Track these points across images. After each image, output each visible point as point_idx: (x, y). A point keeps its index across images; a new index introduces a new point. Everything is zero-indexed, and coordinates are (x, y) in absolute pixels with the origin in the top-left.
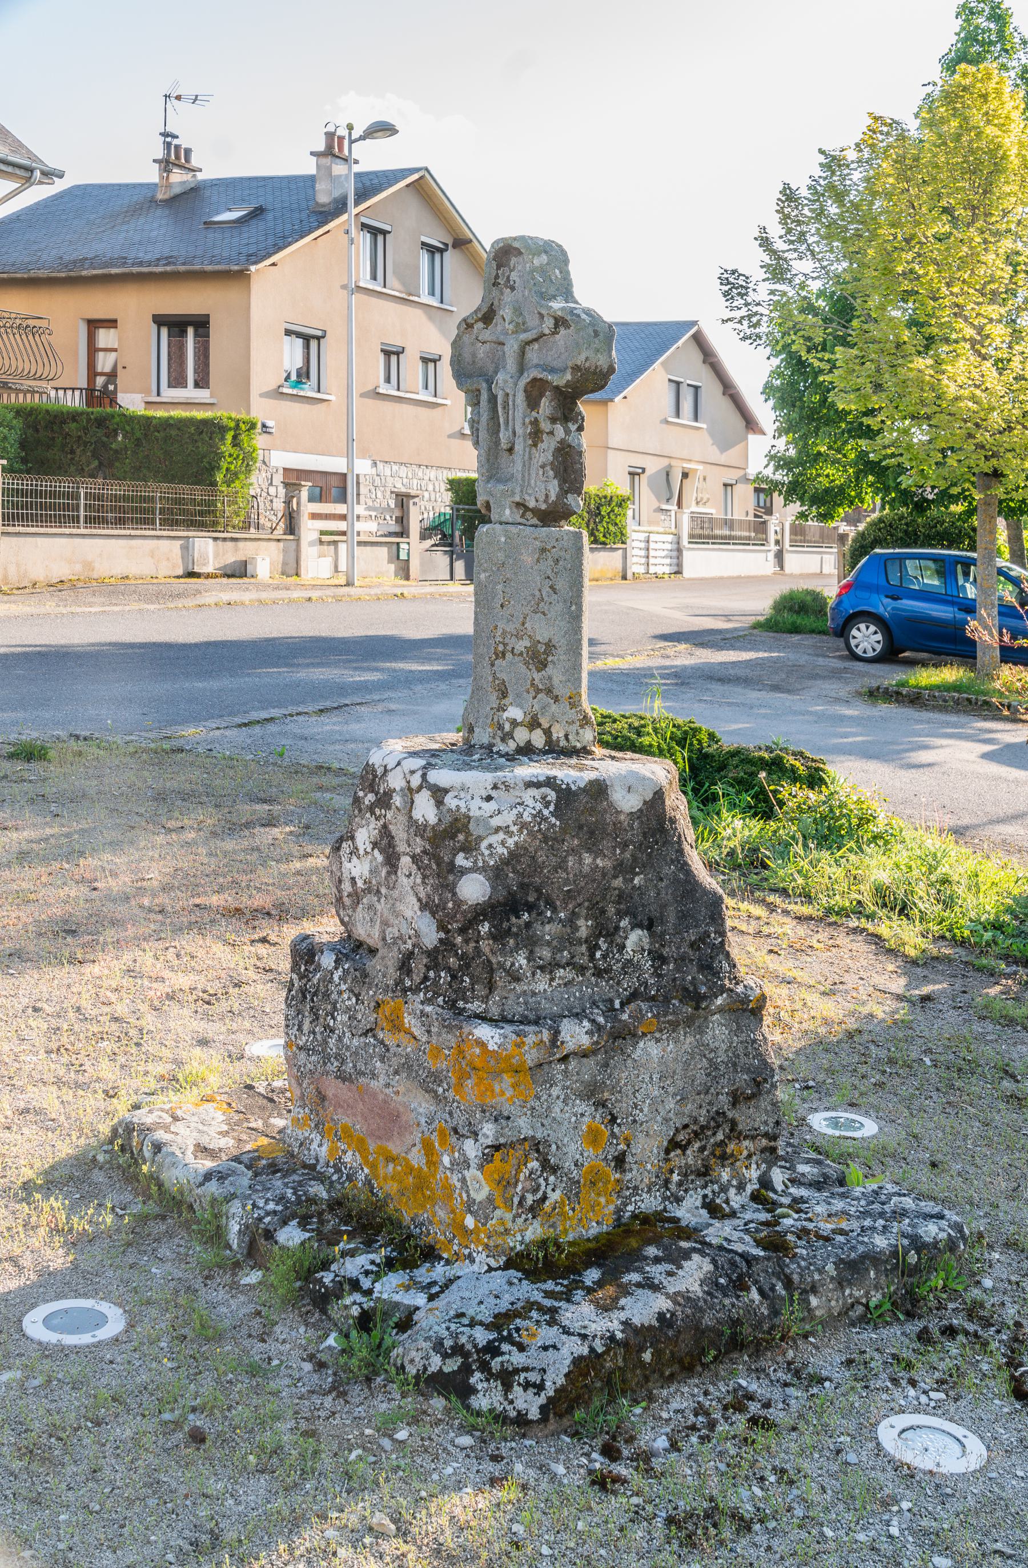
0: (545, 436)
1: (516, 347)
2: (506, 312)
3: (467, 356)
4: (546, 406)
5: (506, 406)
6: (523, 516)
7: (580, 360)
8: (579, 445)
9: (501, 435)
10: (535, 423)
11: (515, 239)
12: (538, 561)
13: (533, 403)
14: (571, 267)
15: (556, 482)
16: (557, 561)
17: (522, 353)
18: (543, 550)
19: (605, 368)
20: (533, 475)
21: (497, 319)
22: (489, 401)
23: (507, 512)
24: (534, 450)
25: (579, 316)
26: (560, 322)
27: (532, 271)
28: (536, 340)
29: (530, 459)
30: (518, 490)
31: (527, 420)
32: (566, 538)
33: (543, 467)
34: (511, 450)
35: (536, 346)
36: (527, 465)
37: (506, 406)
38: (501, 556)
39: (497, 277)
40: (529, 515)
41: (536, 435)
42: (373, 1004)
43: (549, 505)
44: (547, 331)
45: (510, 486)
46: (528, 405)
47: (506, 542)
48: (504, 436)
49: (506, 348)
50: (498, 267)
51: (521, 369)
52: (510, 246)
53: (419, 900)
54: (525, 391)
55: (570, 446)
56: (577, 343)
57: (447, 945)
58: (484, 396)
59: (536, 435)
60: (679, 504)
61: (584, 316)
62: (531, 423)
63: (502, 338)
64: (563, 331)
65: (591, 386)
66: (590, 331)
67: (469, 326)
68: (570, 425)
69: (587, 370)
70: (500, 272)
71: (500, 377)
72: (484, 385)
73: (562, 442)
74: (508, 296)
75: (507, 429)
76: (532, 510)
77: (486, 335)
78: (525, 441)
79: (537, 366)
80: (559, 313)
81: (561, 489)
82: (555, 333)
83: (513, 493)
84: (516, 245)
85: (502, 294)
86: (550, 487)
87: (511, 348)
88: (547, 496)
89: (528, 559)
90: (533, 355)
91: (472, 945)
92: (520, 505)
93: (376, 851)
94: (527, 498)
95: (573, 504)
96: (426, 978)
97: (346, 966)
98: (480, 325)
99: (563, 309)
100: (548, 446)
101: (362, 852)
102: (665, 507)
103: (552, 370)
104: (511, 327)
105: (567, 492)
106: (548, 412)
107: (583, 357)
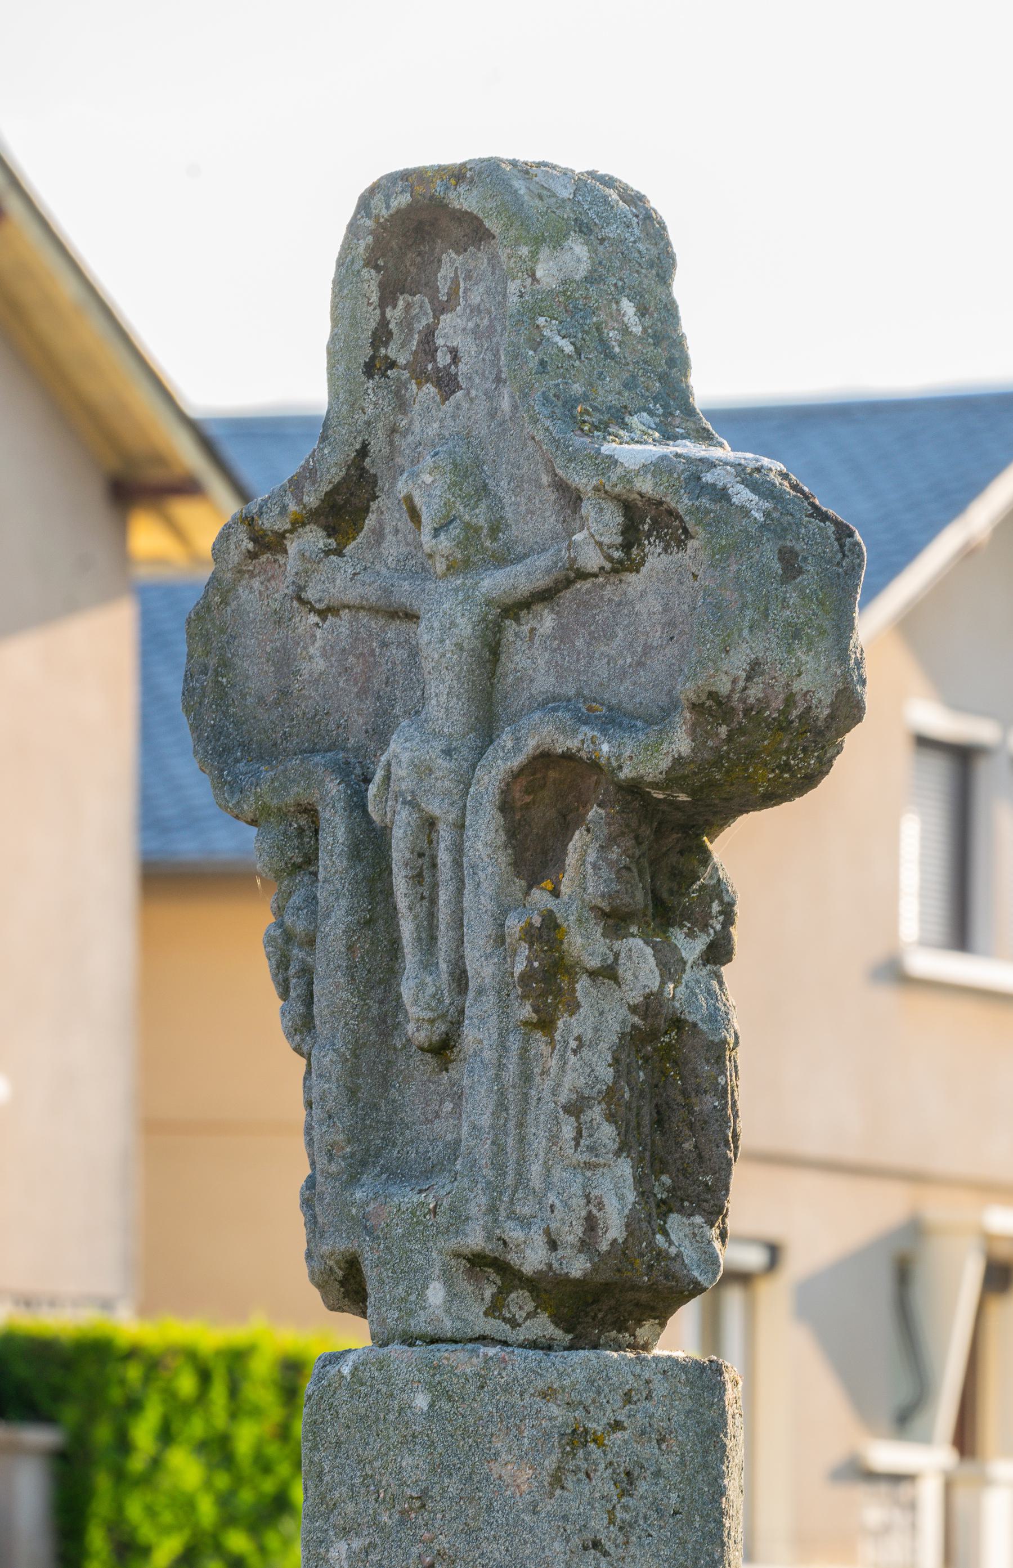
0: (583, 983)
1: (465, 627)
2: (423, 482)
3: (255, 673)
4: (588, 863)
5: (425, 869)
6: (494, 1310)
7: (726, 675)
8: (717, 1018)
9: (407, 989)
10: (546, 933)
11: (458, 174)
12: (557, 1480)
13: (534, 855)
14: (684, 288)
15: (625, 1168)
16: (627, 1481)
17: (491, 652)
18: (577, 1438)
19: (823, 700)
20: (539, 1144)
21: (384, 513)
22: (355, 853)
23: (436, 1294)
24: (540, 1043)
25: (722, 495)
26: (645, 521)
27: (532, 311)
28: (545, 596)
29: (526, 1078)
30: (477, 1204)
31: (514, 924)
32: (660, 1388)
33: (575, 1109)
34: (443, 1049)
35: (547, 621)
36: (514, 1104)
37: (425, 869)
38: (412, 1464)
39: (381, 335)
40: (520, 1302)
41: (549, 983)
43: (601, 1260)
44: (592, 560)
45: (442, 1189)
46: (517, 864)
47: (432, 1413)
48: (417, 991)
49: (424, 635)
50: (388, 296)
51: (487, 721)
52: (439, 206)
54: (505, 807)
55: (678, 1023)
56: (718, 608)
58: (336, 833)
59: (549, 983)
60: (965, 1439)
61: (742, 495)
62: (530, 935)
63: (404, 591)
64: (656, 559)
65: (765, 778)
66: (769, 554)
67: (266, 544)
68: (678, 937)
69: (753, 712)
70: (394, 314)
71: (401, 751)
72: (334, 787)
73: (650, 1006)
74: (428, 416)
75: (428, 965)
76: (533, 1284)
77: (338, 580)
78: (504, 1007)
79: (550, 703)
80: (646, 486)
81: (644, 1195)
82: (625, 562)
83: (459, 1219)
84: (465, 200)
85: (402, 405)
86: (604, 1188)
87: (446, 627)
88: (591, 1224)
89: (516, 1474)
90: (533, 659)
92: (489, 1265)
94: (515, 1234)
95: (690, 1254)
98: (314, 538)
99: (659, 467)
100: (598, 1020)
102: (887, 1455)
103: (613, 719)
104: (444, 544)
105: (665, 1208)
106: (595, 889)
107: (738, 662)
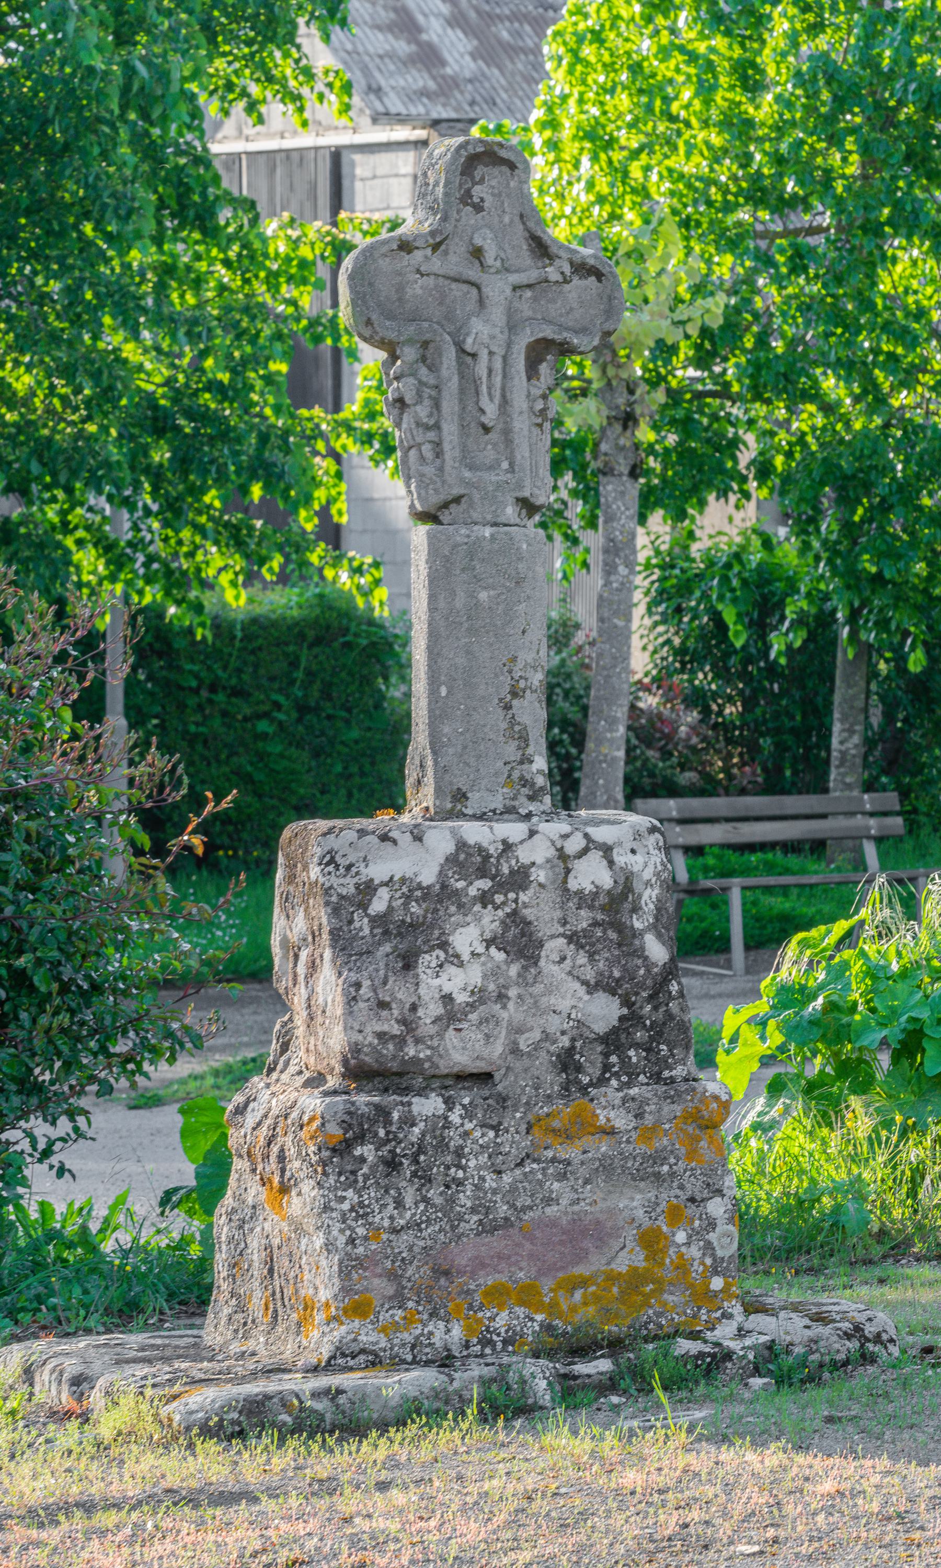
35: (528, 294)
42: (523, 1127)
53: (585, 983)
57: (631, 1019)
91: (662, 1009)
93: (493, 950)
96: (606, 1067)
97: (466, 1101)
101: (466, 957)
